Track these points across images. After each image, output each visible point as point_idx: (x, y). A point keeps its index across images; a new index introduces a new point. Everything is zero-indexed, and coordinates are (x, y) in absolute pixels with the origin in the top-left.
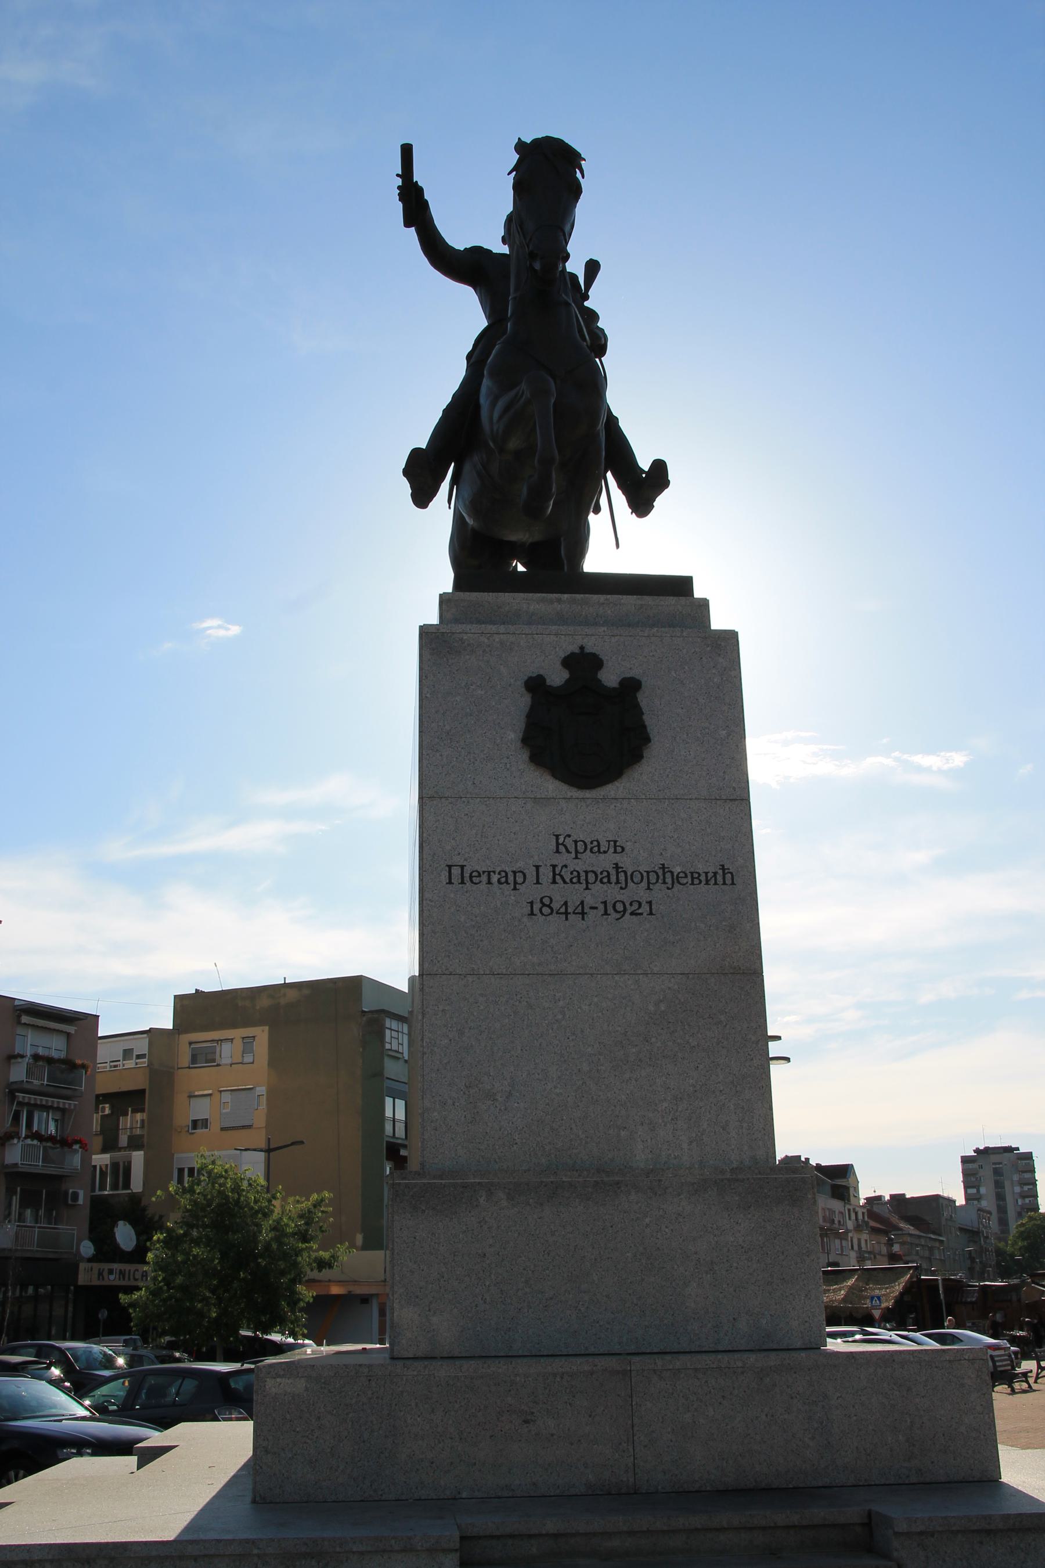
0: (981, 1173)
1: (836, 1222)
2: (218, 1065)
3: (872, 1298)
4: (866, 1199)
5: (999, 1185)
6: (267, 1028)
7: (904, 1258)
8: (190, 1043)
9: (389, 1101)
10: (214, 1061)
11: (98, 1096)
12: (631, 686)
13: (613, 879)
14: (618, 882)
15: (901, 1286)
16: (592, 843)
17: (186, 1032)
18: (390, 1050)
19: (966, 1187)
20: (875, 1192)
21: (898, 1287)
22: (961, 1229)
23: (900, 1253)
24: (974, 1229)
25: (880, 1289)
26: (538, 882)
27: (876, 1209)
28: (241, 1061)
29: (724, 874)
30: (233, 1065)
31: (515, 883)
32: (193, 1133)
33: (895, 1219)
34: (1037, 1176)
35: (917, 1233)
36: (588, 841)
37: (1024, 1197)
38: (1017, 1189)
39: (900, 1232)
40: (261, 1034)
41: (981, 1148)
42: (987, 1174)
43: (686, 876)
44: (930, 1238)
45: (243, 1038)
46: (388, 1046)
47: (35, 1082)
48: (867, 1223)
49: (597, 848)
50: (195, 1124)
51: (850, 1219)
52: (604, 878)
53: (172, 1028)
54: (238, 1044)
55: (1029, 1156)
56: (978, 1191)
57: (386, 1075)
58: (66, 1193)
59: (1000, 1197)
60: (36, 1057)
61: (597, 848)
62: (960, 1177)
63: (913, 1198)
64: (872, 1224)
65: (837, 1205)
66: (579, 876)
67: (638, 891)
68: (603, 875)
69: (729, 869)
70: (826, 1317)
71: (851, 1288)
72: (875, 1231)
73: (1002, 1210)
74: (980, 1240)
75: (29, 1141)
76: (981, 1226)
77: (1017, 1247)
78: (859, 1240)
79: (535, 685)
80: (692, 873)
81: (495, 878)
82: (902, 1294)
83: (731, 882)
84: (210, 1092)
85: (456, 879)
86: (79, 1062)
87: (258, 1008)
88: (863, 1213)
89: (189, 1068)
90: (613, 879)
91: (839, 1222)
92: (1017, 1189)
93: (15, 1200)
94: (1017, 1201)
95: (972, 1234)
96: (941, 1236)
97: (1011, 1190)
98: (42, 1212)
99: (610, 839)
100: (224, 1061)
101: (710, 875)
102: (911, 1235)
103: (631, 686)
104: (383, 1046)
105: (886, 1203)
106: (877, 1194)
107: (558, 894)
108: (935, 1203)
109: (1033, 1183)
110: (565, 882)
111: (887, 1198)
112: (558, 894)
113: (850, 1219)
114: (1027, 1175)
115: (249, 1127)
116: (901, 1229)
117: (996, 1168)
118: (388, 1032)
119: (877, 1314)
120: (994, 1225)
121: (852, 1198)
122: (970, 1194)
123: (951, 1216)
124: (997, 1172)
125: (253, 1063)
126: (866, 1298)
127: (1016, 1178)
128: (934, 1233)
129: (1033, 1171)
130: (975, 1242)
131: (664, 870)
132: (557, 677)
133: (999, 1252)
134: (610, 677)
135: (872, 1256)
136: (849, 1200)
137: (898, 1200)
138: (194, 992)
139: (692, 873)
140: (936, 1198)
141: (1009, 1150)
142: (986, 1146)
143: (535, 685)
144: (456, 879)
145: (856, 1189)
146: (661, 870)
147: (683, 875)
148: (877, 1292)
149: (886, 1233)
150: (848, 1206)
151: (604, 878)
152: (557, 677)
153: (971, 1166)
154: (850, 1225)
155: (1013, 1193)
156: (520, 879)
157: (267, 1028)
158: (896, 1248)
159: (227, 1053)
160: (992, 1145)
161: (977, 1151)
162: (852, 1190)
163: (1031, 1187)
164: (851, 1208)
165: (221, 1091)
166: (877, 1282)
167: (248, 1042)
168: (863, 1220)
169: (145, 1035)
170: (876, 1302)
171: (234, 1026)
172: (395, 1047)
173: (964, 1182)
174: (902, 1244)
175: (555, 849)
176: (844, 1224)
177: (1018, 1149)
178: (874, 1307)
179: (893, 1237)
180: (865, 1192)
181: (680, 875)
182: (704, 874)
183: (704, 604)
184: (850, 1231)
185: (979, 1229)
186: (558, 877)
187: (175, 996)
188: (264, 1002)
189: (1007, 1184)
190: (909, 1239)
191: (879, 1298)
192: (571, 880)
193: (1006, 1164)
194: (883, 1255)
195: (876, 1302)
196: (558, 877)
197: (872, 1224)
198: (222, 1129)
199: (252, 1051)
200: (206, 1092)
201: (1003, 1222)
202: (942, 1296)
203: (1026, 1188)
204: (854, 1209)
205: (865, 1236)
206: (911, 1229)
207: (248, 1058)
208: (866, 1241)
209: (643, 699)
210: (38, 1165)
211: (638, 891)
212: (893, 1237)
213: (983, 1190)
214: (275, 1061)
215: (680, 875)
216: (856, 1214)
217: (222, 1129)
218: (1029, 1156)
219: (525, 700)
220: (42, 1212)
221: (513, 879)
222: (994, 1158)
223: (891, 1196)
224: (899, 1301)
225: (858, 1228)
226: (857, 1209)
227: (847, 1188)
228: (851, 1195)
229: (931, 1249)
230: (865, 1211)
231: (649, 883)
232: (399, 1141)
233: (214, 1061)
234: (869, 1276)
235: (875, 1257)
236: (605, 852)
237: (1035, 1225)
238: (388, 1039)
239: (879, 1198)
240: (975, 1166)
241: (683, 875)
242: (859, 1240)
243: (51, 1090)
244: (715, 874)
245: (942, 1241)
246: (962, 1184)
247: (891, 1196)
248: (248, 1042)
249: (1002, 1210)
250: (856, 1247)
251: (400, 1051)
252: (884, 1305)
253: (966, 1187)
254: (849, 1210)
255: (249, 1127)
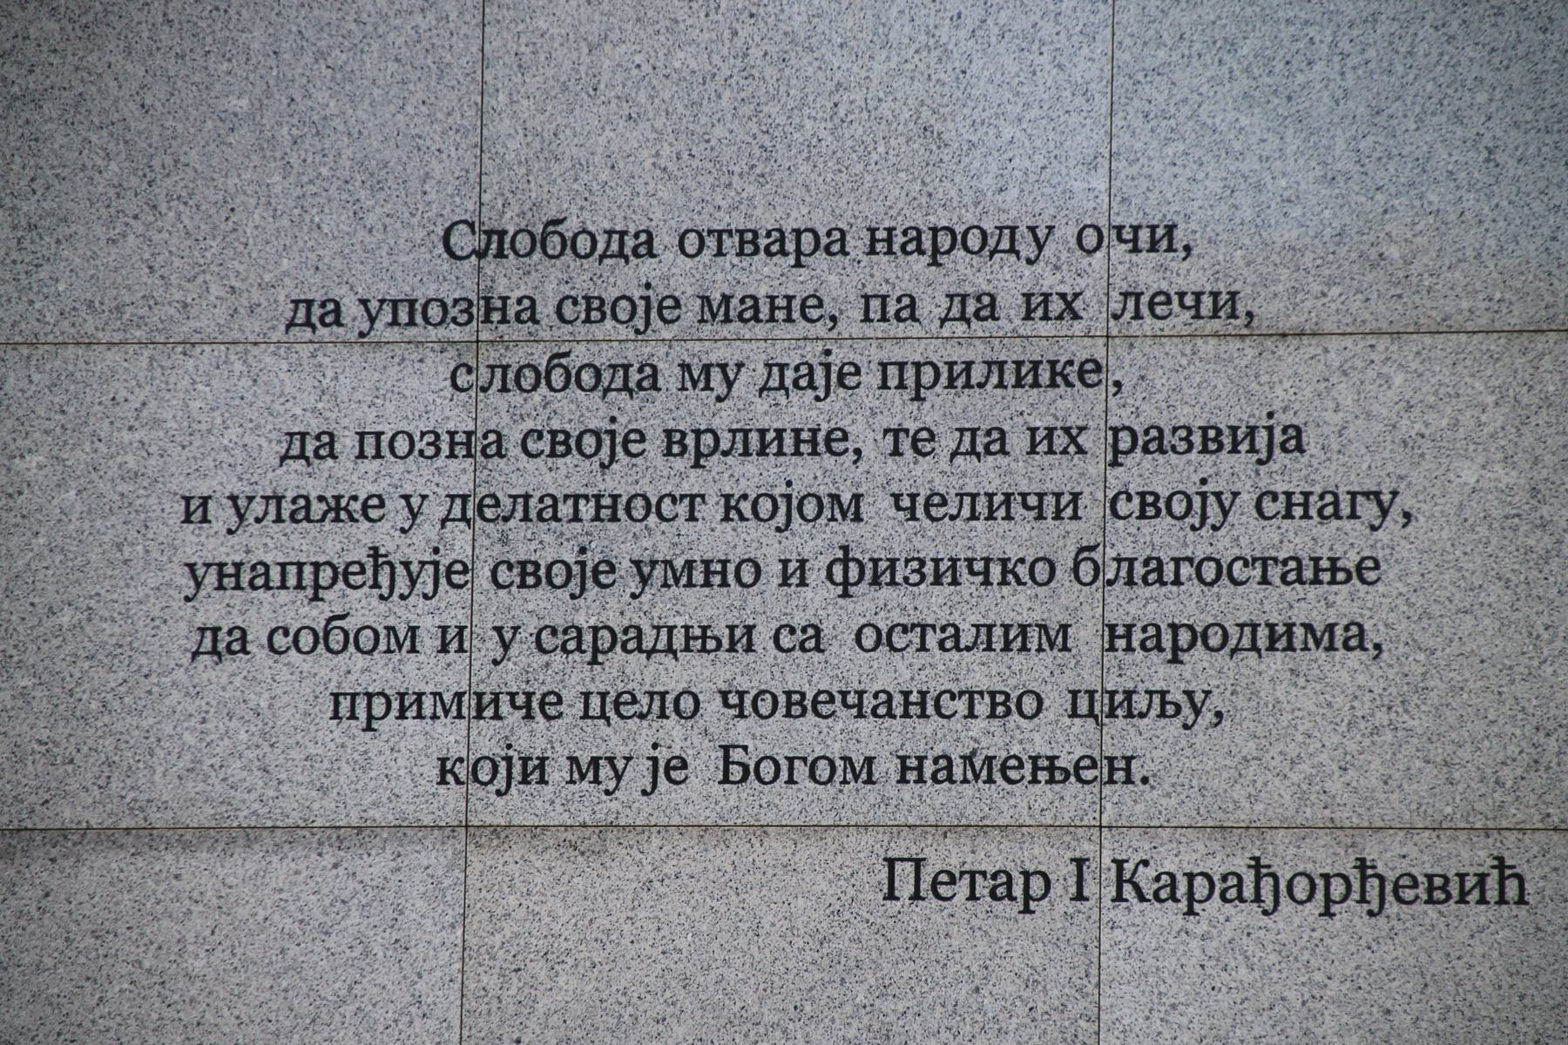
13: (1248, 892)
14: (1258, 899)
16: (1147, 432)
26: (1080, 896)
29: (1502, 881)
31: (1027, 897)
36: (1139, 429)
43: (1415, 885)
66: (1173, 885)
68: (1162, 883)
69: (1269, 867)
80: (1430, 877)
81: (982, 886)
83: (373, 452)
85: (905, 889)
90: (1248, 892)
99: (1357, 489)
101: (1470, 882)
110: (1142, 898)
131: (376, 561)
139: (1430, 877)
144: (905, 889)
146: (1253, 872)
147: (852, 369)
156: (1037, 885)
175: (1069, 707)
181: (666, 303)
182: (279, 568)
186: (1127, 888)
192: (1156, 895)
196: (1127, 888)
215: (666, 303)
231: (1328, 900)
236: (981, 385)
241: (852, 369)
244: (1482, 878)
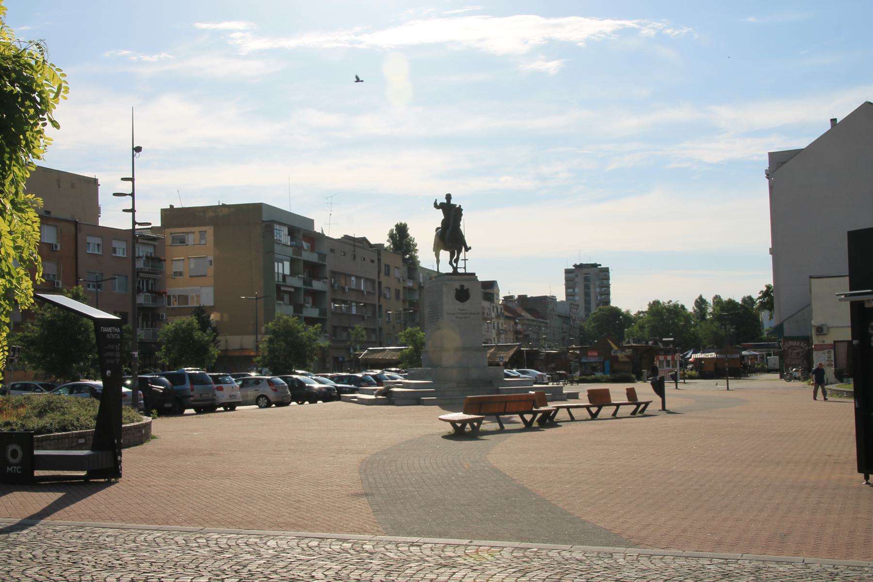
0: (577, 279)
1: (486, 313)
2: (187, 245)
3: (500, 358)
4: (504, 297)
5: (587, 287)
6: (212, 227)
7: (523, 333)
8: (171, 234)
9: (276, 264)
10: (184, 242)
11: (175, 272)
12: (468, 289)
15: (513, 352)
17: (169, 227)
18: (277, 240)
19: (568, 287)
20: (509, 293)
21: (511, 352)
22: (559, 316)
23: (521, 330)
24: (567, 315)
25: (503, 354)
27: (509, 304)
28: (199, 243)
30: (195, 246)
32: (175, 278)
33: (519, 310)
34: (611, 282)
35: (532, 318)
37: (601, 295)
38: (598, 290)
39: (522, 318)
40: (210, 230)
41: (578, 264)
42: (580, 281)
44: (540, 321)
45: (200, 232)
46: (275, 238)
47: (147, 268)
48: (503, 314)
49: (463, 310)
50: (176, 274)
51: (493, 311)
52: (464, 314)
53: (160, 225)
54: (197, 235)
55: (606, 270)
56: (574, 290)
57: (275, 252)
58: (159, 315)
59: (587, 294)
60: (147, 257)
61: (463, 310)
62: (563, 281)
63: (532, 298)
64: (506, 314)
65: (486, 304)
67: (468, 315)
70: (145, 415)
71: (492, 353)
72: (507, 317)
73: (587, 302)
74: (570, 322)
75: (147, 294)
76: (571, 313)
77: (590, 326)
78: (498, 323)
79: (456, 289)
82: (513, 356)
84: (183, 258)
86: (162, 258)
87: (207, 216)
88: (501, 308)
89: (171, 246)
91: (487, 313)
92: (598, 290)
93: (140, 319)
94: (597, 297)
95: (566, 318)
96: (546, 319)
97: (595, 290)
98: (149, 323)
100: (189, 243)
102: (528, 320)
103: (468, 289)
104: (274, 238)
105: (515, 301)
106: (511, 294)
107: (459, 316)
108: (545, 301)
109: (608, 286)
111: (516, 297)
112: (459, 316)
113: (493, 311)
114: (605, 282)
115: (205, 276)
116: (522, 316)
117: (586, 277)
118: (275, 230)
119: (501, 363)
120: (582, 312)
121: (495, 300)
122: (569, 293)
123: (553, 308)
124: (586, 279)
125: (205, 244)
126: (497, 357)
127: (597, 283)
128: (542, 318)
129: (608, 279)
130: (567, 323)
132: (459, 288)
133: (581, 329)
134: (465, 288)
135: (505, 332)
136: (493, 301)
137: (523, 298)
138: (169, 207)
140: (544, 298)
141: (595, 266)
142: (581, 263)
143: (456, 289)
145: (498, 295)
148: (502, 355)
149: (513, 319)
150: (493, 305)
151: (464, 314)
152: (459, 288)
153: (570, 275)
154: (493, 315)
155: (595, 292)
157: (212, 227)
158: (519, 327)
159: (191, 239)
160: (584, 263)
161: (575, 266)
162: (495, 295)
163: (606, 288)
164: (494, 305)
165: (189, 258)
166: (502, 351)
167: (203, 234)
168: (501, 312)
169: (149, 230)
170: (501, 359)
171: (194, 225)
172: (278, 239)
173: (566, 285)
174: (523, 325)
176: (490, 314)
177: (600, 265)
178: (500, 361)
179: (517, 321)
180: (503, 294)
183: (477, 277)
184: (493, 318)
185: (570, 315)
187: (162, 210)
188: (211, 214)
189: (592, 287)
190: (527, 322)
191: (503, 357)
193: (592, 275)
194: (511, 332)
195: (501, 359)
197: (506, 314)
198: (191, 277)
199: (204, 238)
200: (181, 258)
201: (588, 309)
202: (525, 357)
203: (603, 289)
204: (496, 306)
205: (501, 321)
206: (529, 316)
207: (203, 242)
208: (502, 324)
209: (469, 291)
210: (150, 304)
211: (468, 315)
212: (517, 321)
213: (577, 290)
214: (217, 243)
216: (497, 309)
217: (191, 277)
218: (606, 270)
219: (455, 291)
220: (149, 323)
221: (454, 314)
222: (586, 271)
223: (519, 296)
224: (511, 359)
225: (498, 317)
226: (498, 306)
227: (493, 295)
228: (495, 298)
229: (540, 327)
230: (502, 307)
232: (281, 283)
233: (184, 242)
234: (499, 348)
235: (506, 333)
237: (602, 314)
238: (275, 234)
239: (512, 297)
240: (573, 275)
242: (498, 323)
243: (152, 271)
245: (547, 323)
246: (564, 286)
247: (519, 296)
248: (203, 234)
249: (587, 302)
250: (496, 327)
251: (281, 240)
252: (504, 360)
253: (567, 288)
254: (493, 307)
255: (205, 276)
